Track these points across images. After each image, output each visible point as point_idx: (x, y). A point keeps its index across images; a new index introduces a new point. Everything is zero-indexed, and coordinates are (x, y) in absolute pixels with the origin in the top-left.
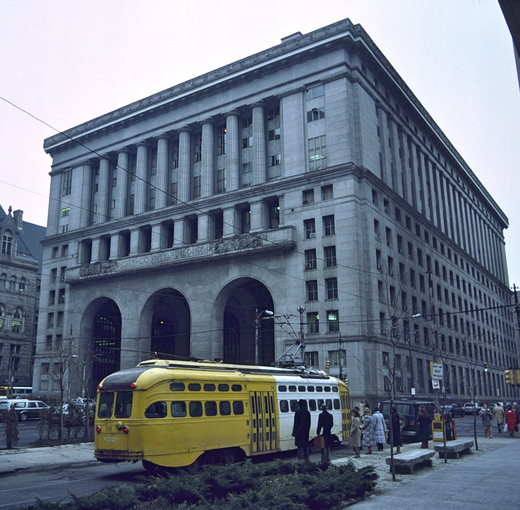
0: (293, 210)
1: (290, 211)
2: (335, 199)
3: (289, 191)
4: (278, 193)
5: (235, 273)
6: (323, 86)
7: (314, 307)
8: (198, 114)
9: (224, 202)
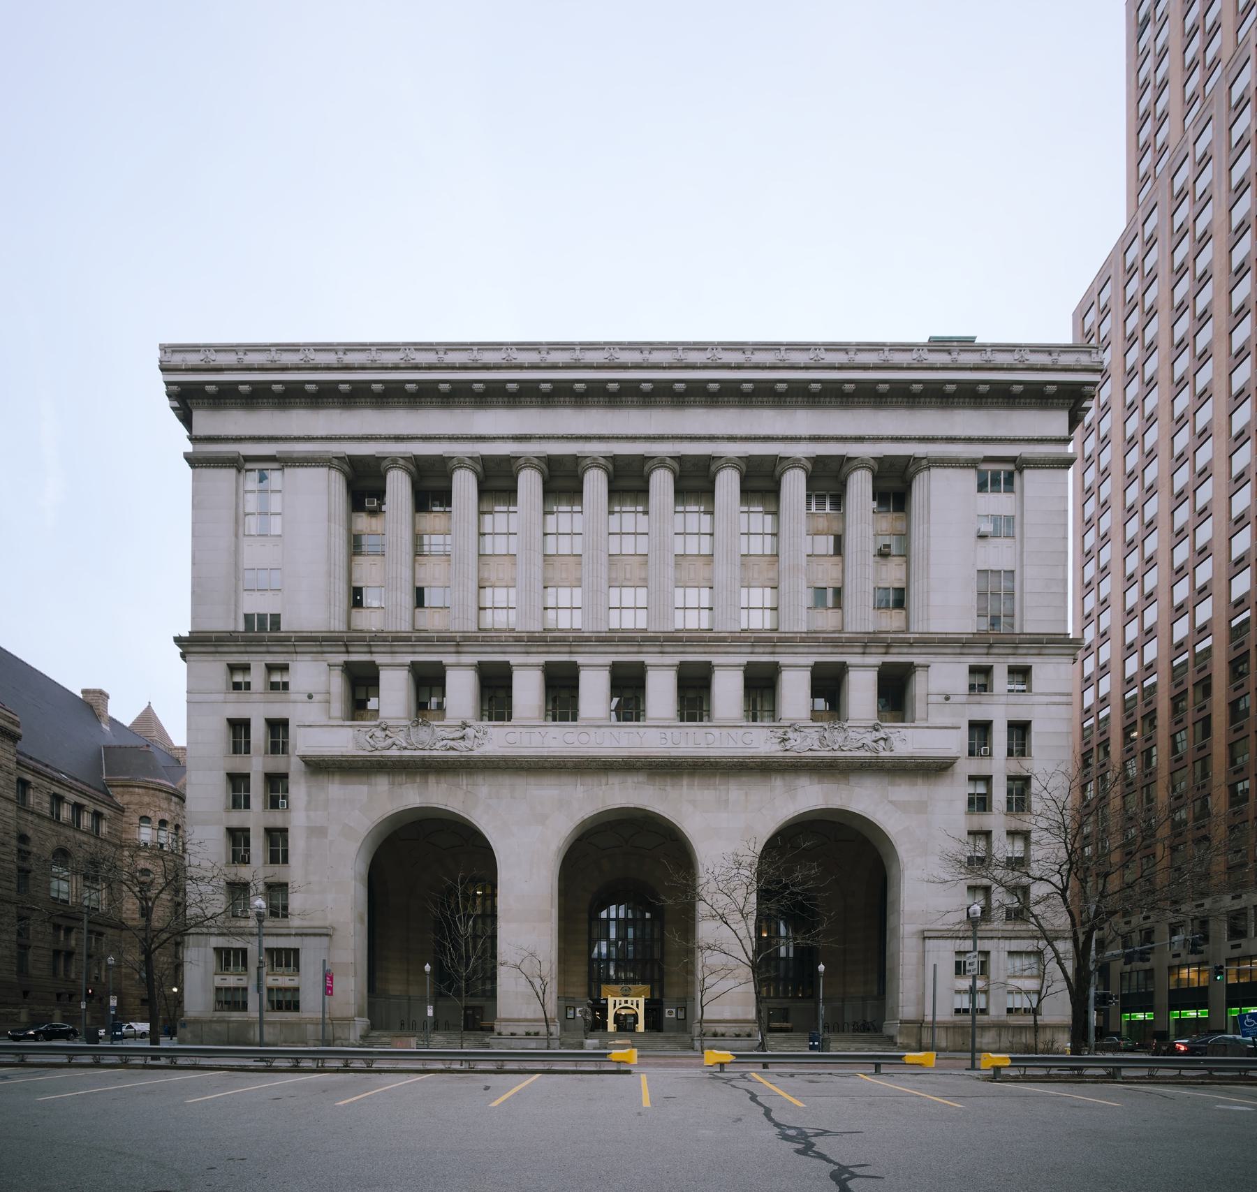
0: (947, 698)
1: (941, 699)
2: (1037, 694)
3: (940, 658)
4: (917, 660)
5: (811, 796)
6: (279, 473)
7: (244, 873)
8: (859, 439)
9: (720, 649)
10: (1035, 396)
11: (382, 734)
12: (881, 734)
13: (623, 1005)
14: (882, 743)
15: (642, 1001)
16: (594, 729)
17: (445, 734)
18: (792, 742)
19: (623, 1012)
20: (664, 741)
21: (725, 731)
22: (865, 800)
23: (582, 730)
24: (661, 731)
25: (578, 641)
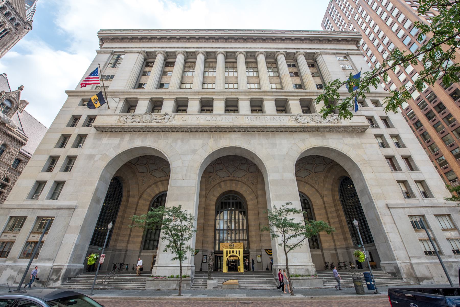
10: (347, 41)
13: (232, 254)
14: (336, 120)
15: (241, 250)
17: (157, 118)
19: (232, 258)
22: (257, 146)
23: (213, 116)
24: (244, 115)
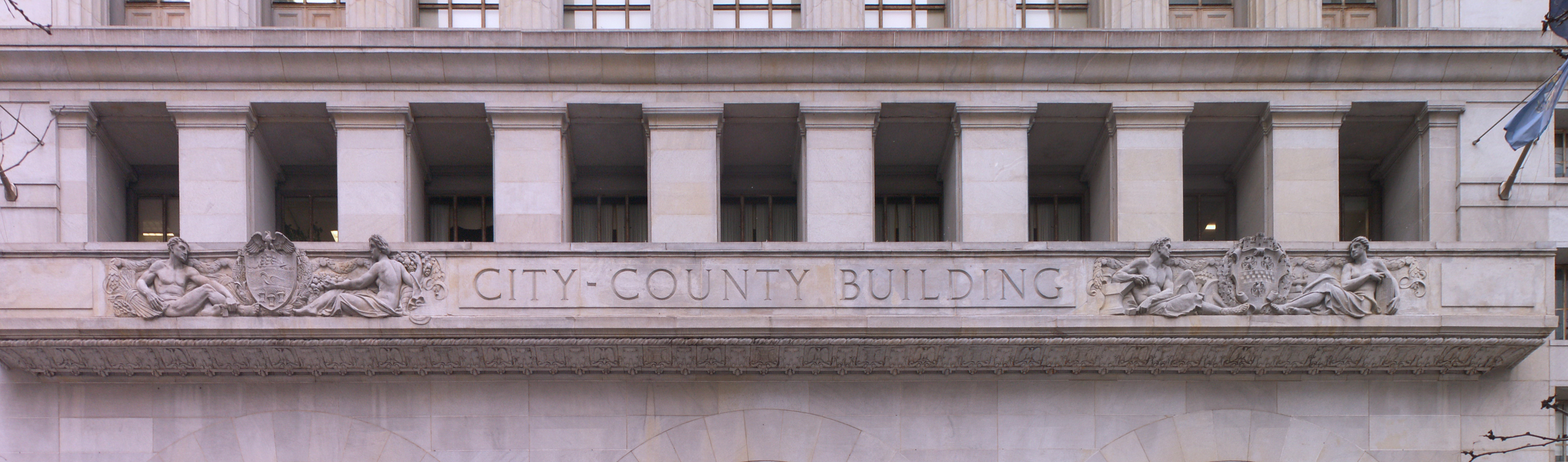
4: (1435, 98)
11: (179, 276)
12: (1367, 269)
14: (1368, 292)
16: (686, 262)
17: (329, 276)
18: (1155, 293)
20: (851, 291)
21: (995, 265)
23: (654, 263)
25: (646, 61)
